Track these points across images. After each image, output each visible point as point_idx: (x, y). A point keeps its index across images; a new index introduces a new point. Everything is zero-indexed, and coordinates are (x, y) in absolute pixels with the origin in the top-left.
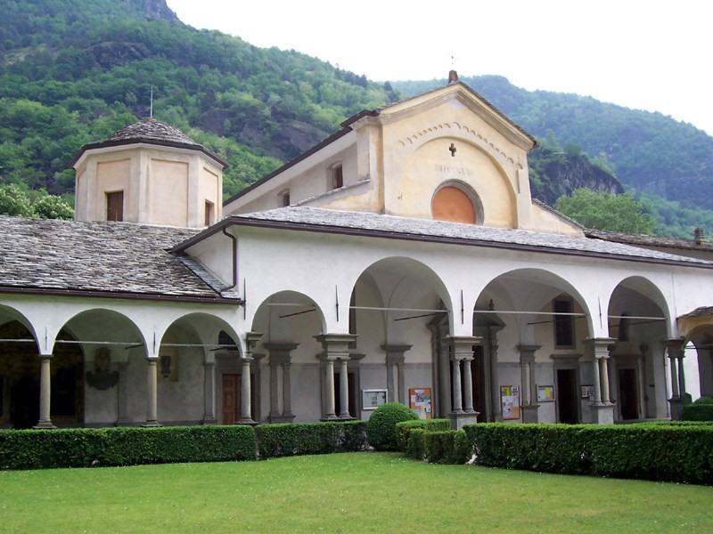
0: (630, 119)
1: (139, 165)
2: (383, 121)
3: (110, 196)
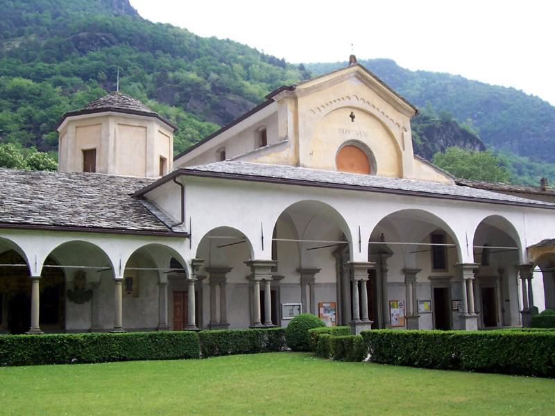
0: (490, 93)
1: (108, 129)
2: (298, 95)
3: (85, 152)
